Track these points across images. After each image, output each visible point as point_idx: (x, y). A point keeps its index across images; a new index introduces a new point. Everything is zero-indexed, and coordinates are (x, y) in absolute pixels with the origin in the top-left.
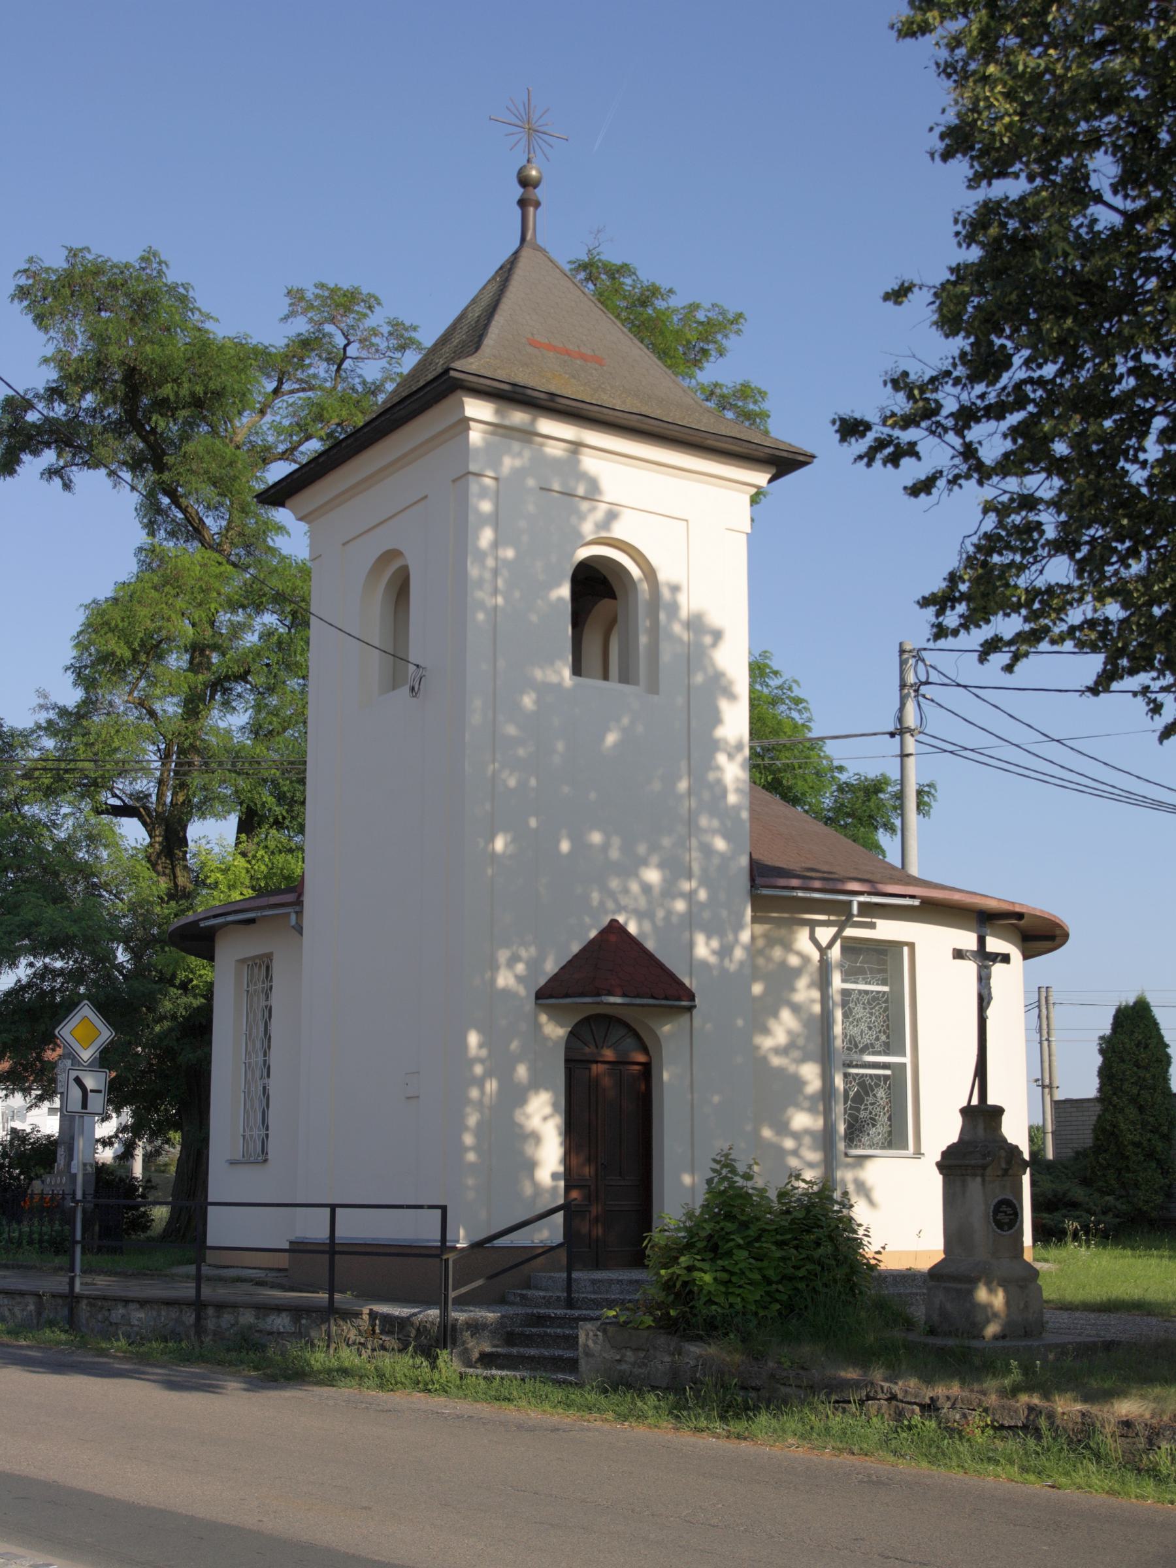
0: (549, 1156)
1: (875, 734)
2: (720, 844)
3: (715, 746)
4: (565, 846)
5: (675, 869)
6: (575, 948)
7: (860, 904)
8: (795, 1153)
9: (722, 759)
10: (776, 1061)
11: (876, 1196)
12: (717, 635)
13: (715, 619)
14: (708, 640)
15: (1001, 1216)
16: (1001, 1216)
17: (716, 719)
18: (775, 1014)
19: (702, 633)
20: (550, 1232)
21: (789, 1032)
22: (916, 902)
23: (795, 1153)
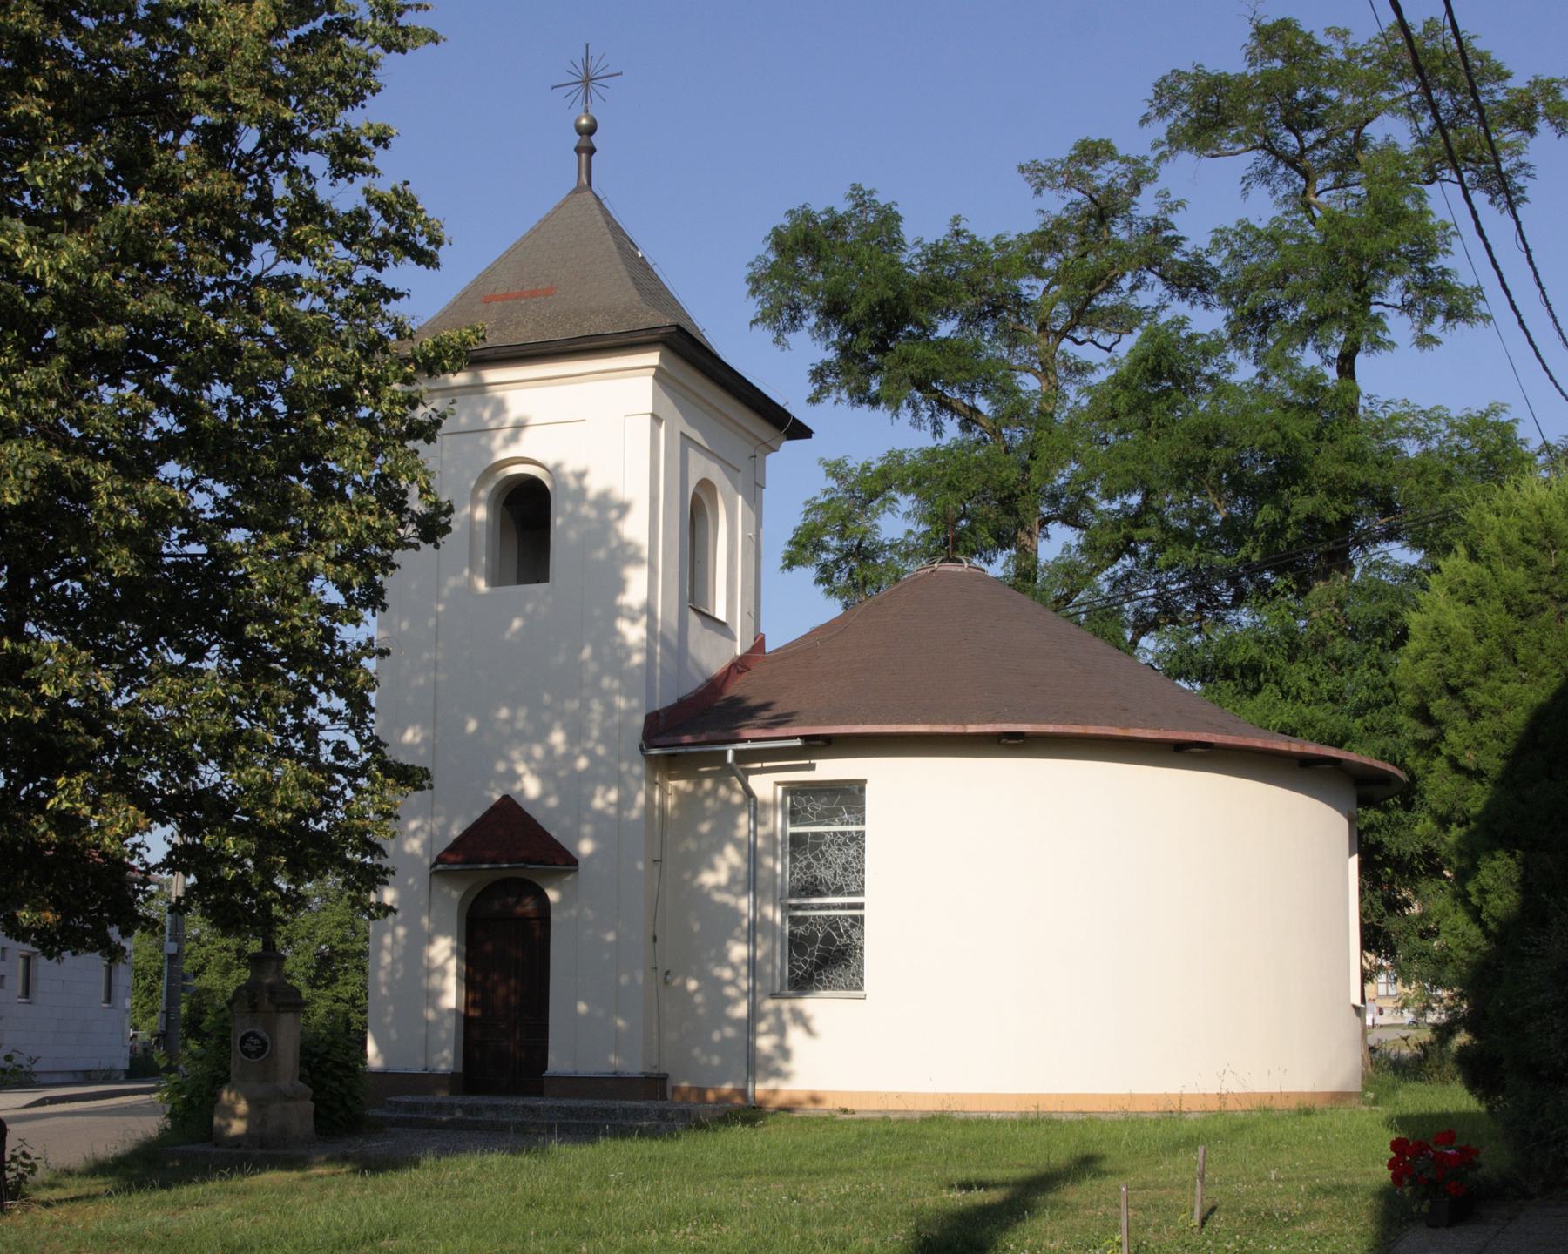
0: (451, 996)
1: (1496, 267)
2: (621, 702)
3: (617, 612)
4: (472, 726)
5: (576, 735)
6: (477, 814)
7: (736, 752)
8: (733, 983)
9: (623, 625)
10: (719, 897)
11: (816, 1025)
12: (624, 508)
13: (622, 493)
14: (613, 514)
15: (247, 1046)
16: (247, 1046)
17: (620, 586)
18: (719, 849)
19: (611, 507)
20: (445, 1059)
21: (732, 869)
22: (798, 743)
23: (733, 983)
